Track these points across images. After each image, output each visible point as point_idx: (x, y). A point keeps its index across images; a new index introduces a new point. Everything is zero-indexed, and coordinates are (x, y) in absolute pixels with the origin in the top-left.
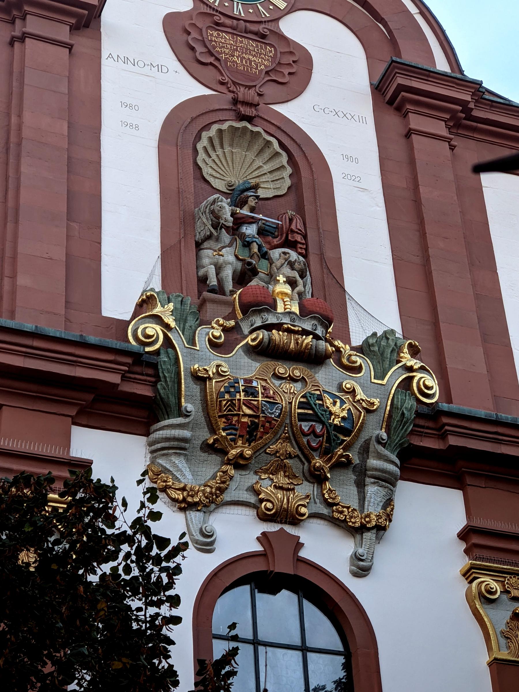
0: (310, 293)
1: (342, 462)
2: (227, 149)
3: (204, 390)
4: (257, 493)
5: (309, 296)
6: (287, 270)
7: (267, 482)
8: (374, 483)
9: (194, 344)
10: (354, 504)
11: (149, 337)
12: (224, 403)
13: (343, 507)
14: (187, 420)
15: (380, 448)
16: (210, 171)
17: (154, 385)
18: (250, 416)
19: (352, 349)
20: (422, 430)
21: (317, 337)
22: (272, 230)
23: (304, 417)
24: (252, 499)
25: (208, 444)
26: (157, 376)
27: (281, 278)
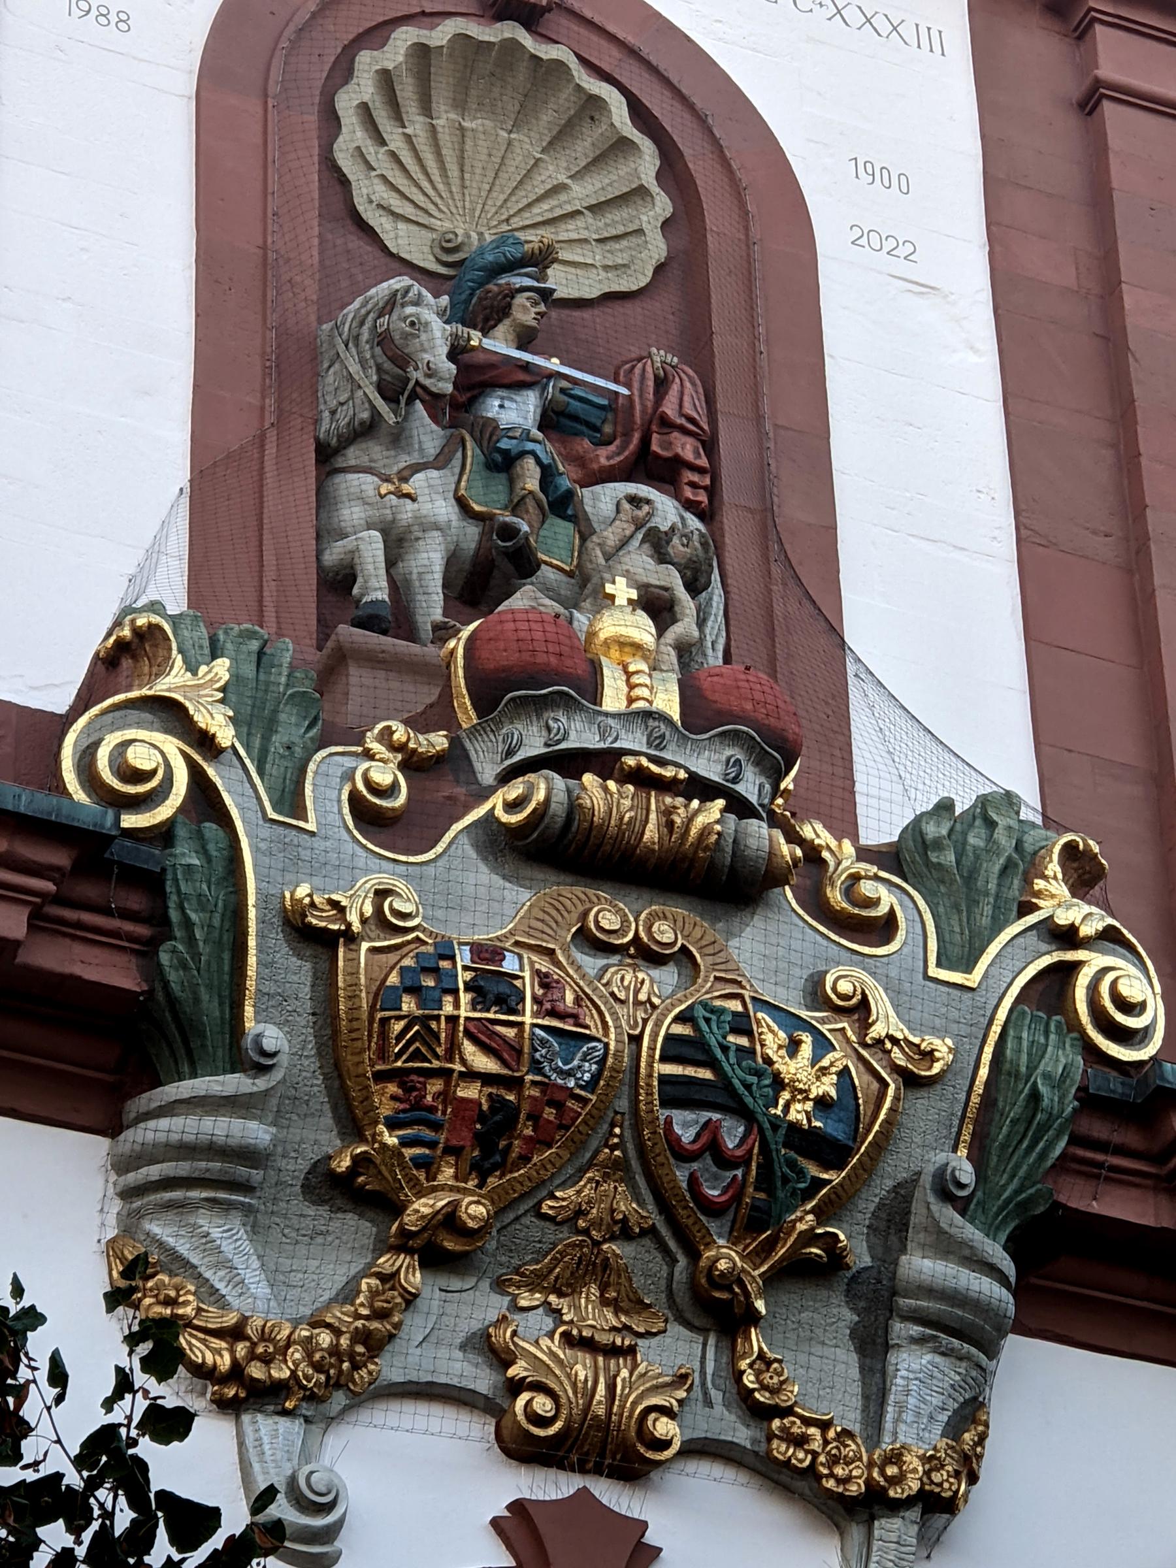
0: (720, 647)
1: (812, 1260)
2: (445, 117)
3: (326, 980)
4: (502, 1358)
5: (715, 659)
6: (640, 561)
7: (539, 1321)
8: (920, 1341)
9: (300, 812)
10: (848, 1415)
11: (139, 776)
12: (398, 1027)
13: (807, 1422)
14: (262, 1083)
15: (948, 1216)
16: (381, 193)
17: (146, 951)
18: (487, 1079)
19: (864, 853)
20: (1100, 1157)
21: (739, 807)
22: (594, 417)
23: (679, 1092)
24: (483, 1380)
25: (334, 1178)
26: (160, 921)
27: (622, 590)
